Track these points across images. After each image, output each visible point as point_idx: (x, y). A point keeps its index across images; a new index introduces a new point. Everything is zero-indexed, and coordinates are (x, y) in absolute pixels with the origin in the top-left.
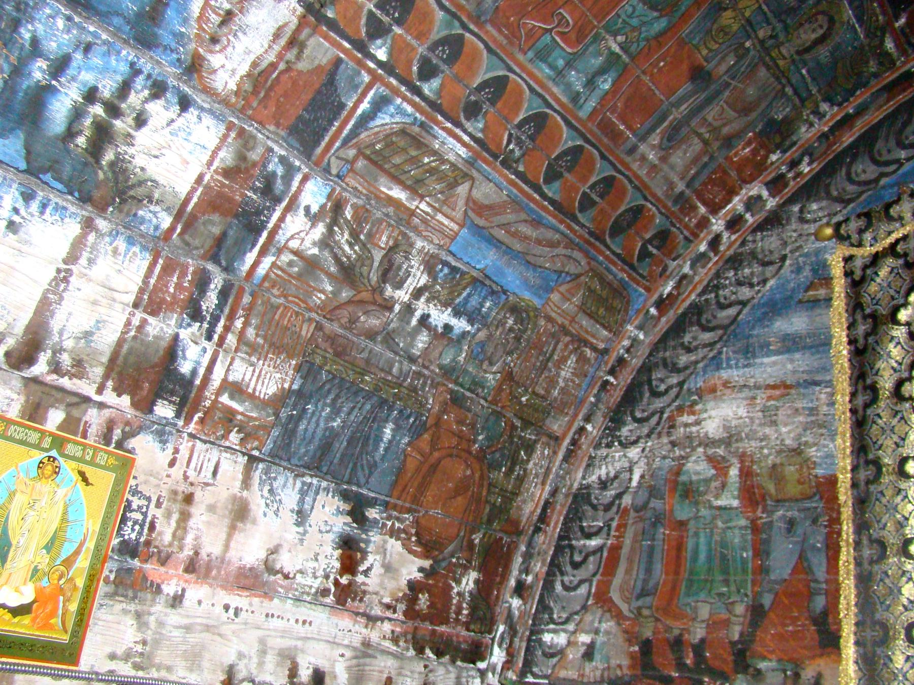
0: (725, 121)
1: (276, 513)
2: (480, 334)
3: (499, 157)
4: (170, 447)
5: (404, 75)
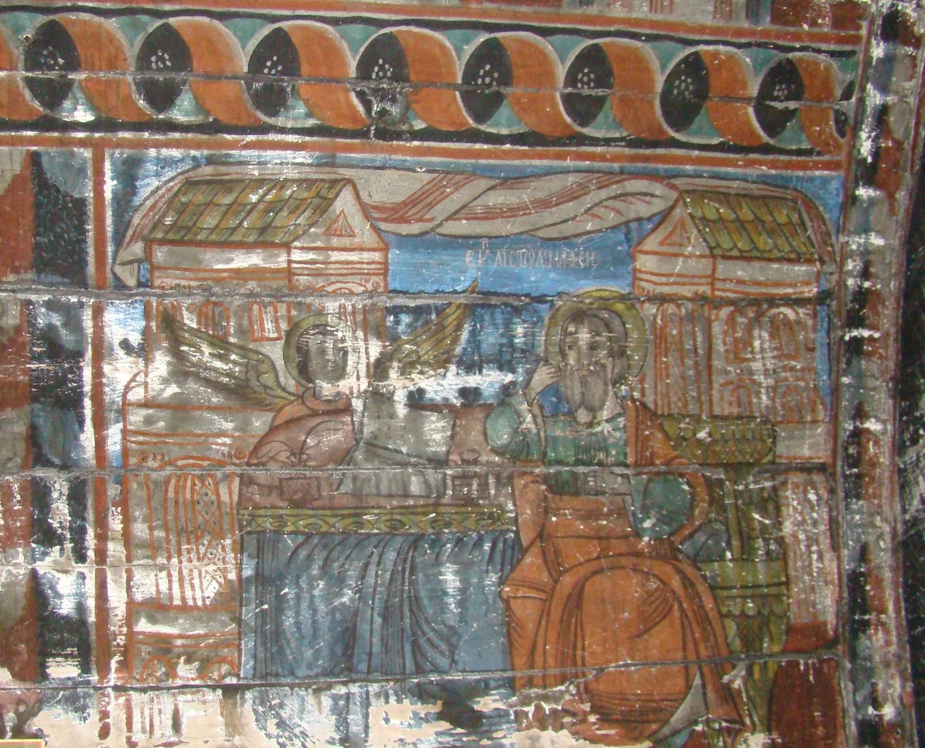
2: (536, 377)
3: (369, 131)
4: (93, 714)
5: (133, 118)
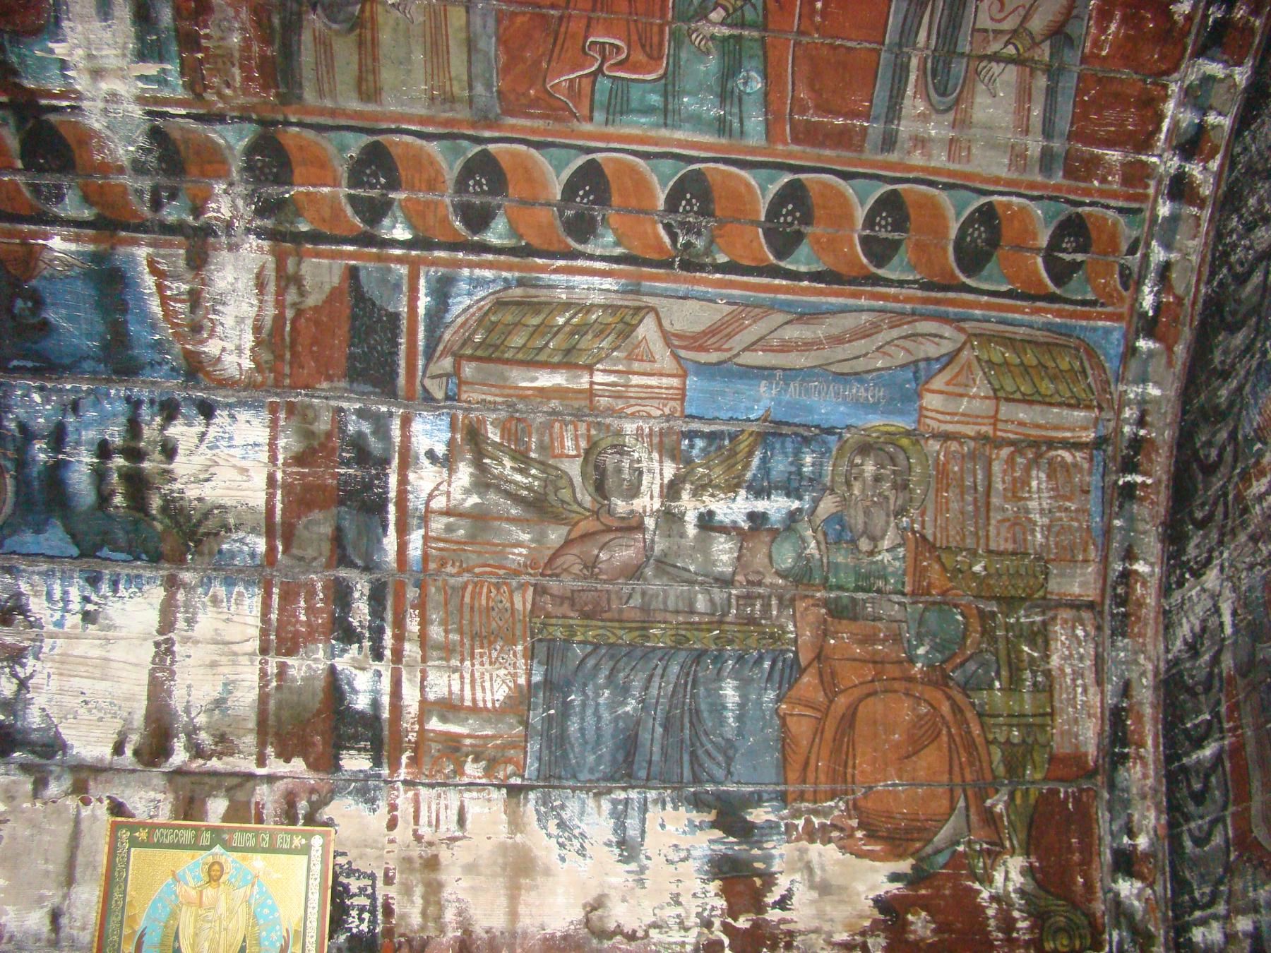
0: (1022, 12)
1: (582, 852)
2: (822, 505)
3: (673, 262)
4: (383, 806)
